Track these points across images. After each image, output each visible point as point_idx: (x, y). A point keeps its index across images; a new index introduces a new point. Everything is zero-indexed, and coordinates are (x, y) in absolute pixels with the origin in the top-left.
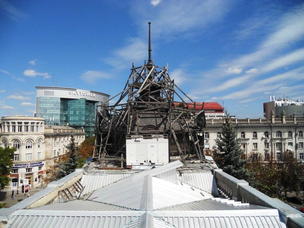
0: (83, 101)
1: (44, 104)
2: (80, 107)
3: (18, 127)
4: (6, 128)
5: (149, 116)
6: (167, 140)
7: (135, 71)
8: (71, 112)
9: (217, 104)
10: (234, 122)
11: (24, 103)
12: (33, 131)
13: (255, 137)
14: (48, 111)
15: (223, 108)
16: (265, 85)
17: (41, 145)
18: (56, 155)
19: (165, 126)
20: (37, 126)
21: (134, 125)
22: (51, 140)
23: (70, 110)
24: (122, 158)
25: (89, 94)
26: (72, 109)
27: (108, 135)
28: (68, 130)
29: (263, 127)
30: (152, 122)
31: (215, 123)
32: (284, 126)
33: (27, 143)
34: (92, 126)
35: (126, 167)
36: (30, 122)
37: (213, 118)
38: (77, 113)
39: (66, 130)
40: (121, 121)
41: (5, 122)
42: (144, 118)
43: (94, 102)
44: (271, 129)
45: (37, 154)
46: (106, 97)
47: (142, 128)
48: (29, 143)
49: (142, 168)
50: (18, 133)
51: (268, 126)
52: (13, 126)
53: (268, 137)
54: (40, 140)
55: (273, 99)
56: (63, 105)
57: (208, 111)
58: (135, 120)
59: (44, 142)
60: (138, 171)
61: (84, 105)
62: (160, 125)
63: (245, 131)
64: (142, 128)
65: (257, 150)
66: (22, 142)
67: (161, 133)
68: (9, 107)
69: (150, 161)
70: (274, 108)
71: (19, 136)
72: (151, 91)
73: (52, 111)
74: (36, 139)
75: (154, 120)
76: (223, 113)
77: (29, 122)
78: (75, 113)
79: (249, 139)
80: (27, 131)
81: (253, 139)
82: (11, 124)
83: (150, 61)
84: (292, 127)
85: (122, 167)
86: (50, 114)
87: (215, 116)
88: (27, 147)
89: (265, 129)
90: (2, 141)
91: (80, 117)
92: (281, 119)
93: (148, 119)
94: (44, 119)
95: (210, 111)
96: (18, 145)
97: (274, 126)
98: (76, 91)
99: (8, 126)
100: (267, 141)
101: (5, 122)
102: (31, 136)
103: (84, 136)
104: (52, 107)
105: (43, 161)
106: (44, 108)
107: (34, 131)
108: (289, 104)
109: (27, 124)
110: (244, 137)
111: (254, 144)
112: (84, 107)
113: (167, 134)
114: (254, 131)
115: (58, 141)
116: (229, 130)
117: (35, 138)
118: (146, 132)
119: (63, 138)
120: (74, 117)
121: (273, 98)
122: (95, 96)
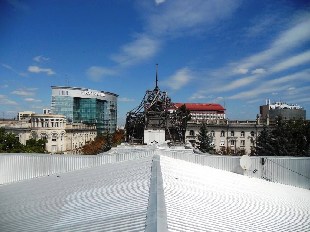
0: (94, 100)
1: (59, 103)
2: (91, 106)
3: (40, 123)
4: (36, 124)
5: (156, 119)
6: (164, 131)
7: (149, 93)
8: (83, 111)
9: (219, 105)
10: (226, 123)
11: (27, 99)
12: (57, 127)
13: (243, 135)
14: (62, 109)
15: (224, 109)
16: (275, 86)
17: (63, 138)
18: (75, 148)
19: (164, 124)
20: (61, 123)
21: (148, 124)
22: (70, 135)
23: (82, 109)
24: (142, 140)
25: (99, 94)
26: (84, 108)
28: (83, 127)
29: (249, 127)
30: (157, 122)
31: (210, 123)
32: (218, 127)
33: (52, 136)
34: (101, 124)
35: (144, 144)
36: (55, 119)
37: (207, 118)
38: (89, 111)
39: (82, 127)
41: (35, 118)
42: (153, 120)
43: (103, 102)
44: (257, 129)
45: (60, 146)
46: (115, 97)
47: (151, 125)
48: (54, 136)
49: (152, 144)
50: (41, 128)
51: (254, 127)
52: (41, 122)
53: (253, 136)
54: (63, 134)
55: (268, 102)
56: (76, 104)
57: (210, 111)
58: (148, 121)
59: (65, 136)
60: (149, 145)
61: (95, 104)
62: (161, 124)
63: (234, 130)
64: (151, 125)
65: (244, 146)
66: (49, 135)
67: (162, 128)
68: (12, 102)
69: (156, 141)
70: (269, 112)
71: (47, 131)
72: (157, 105)
73: (66, 109)
74: (59, 133)
75: (158, 121)
76: (225, 114)
77: (54, 119)
78: (86, 111)
79: (238, 137)
80: (53, 127)
81: (241, 137)
82: (40, 121)
83: (157, 86)
84: (246, 128)
85: (142, 144)
86: (65, 111)
87: (209, 117)
88: (52, 139)
89: (251, 129)
90: (32, 134)
91: (91, 115)
92: (265, 121)
93: (155, 121)
94: (65, 117)
95: (212, 112)
96: (46, 138)
97: (259, 127)
98: (87, 91)
99: (38, 123)
100: (253, 139)
101: (35, 118)
102: (56, 131)
103: (96, 133)
104: (66, 105)
105: (65, 152)
106: (59, 106)
107: (58, 127)
108: (282, 108)
109: (53, 121)
110: (234, 135)
111: (242, 141)
112: (95, 106)
113: (165, 128)
114: (242, 130)
115: (76, 136)
116: (204, 128)
117: (59, 132)
118: (154, 127)
119: (80, 133)
120: (86, 115)
122: (105, 95)
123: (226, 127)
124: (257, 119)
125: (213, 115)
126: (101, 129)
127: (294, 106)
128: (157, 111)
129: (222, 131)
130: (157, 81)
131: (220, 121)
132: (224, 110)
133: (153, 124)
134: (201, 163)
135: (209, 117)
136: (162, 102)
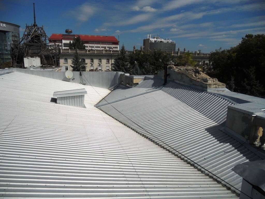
5: (35, 49)
9: (113, 38)
27: (17, 56)
34: (5, 54)
40: (22, 51)
55: (149, 37)
57: (107, 43)
62: (39, 53)
63: (93, 58)
72: (35, 38)
75: (37, 51)
83: (35, 23)
121: (150, 36)
123: (111, 56)
124: (134, 50)
125: (103, 46)
126: (6, 58)
127: (168, 41)
128: (36, 42)
129: (115, 58)
130: (35, 18)
131: (106, 51)
132: (118, 41)
133: (32, 53)
134: (43, 75)
135: (100, 47)
136: (39, 35)
